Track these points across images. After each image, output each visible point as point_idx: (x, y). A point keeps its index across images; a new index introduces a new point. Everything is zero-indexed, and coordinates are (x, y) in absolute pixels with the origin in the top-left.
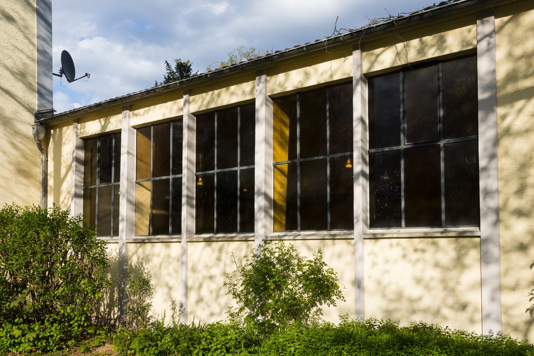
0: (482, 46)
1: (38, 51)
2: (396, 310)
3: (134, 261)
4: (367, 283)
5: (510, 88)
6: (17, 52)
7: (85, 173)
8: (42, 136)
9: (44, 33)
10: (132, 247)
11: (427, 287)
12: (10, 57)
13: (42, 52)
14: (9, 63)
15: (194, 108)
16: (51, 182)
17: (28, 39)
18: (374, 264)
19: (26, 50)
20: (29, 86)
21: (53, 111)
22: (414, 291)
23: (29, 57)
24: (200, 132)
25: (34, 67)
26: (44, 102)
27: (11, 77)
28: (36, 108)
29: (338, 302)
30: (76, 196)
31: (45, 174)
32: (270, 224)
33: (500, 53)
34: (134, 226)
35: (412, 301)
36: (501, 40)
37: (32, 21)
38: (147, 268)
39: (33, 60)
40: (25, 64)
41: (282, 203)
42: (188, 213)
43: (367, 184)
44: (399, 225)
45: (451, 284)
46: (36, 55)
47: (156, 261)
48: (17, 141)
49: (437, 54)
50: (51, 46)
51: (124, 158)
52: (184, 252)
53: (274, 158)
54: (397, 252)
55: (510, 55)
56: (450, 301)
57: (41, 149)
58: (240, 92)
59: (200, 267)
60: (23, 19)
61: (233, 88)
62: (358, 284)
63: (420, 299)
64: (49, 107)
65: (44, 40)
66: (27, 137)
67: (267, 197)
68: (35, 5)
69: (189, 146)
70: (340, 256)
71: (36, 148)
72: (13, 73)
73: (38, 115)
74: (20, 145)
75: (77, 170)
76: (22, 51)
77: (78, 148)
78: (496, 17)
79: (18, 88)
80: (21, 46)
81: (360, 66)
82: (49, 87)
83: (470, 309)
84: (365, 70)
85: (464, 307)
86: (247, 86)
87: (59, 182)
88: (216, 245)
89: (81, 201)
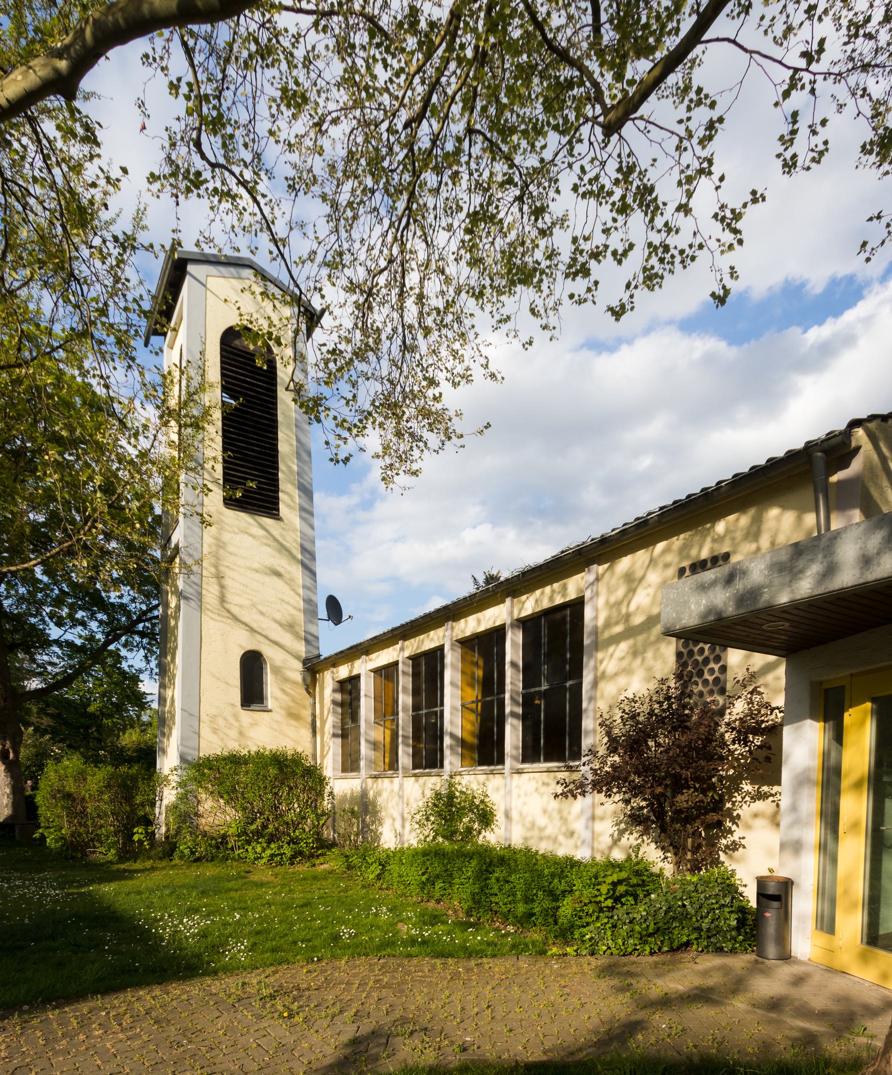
0: (588, 594)
1: (304, 600)
2: (531, 838)
3: (371, 794)
4: (515, 815)
5: (606, 635)
6: (284, 605)
7: (342, 714)
8: (309, 680)
9: (309, 582)
10: (370, 781)
11: (550, 818)
12: (279, 611)
13: (308, 601)
14: (278, 616)
15: (407, 654)
16: (318, 724)
17: (294, 590)
18: (519, 796)
19: (292, 601)
20: (296, 635)
21: (319, 656)
22: (542, 821)
23: (295, 608)
24: (416, 675)
25: (300, 617)
26: (310, 648)
27: (279, 629)
28: (304, 655)
29: (496, 829)
30: (334, 735)
31: (314, 716)
32: (457, 761)
33: (601, 601)
34: (371, 763)
35: (541, 829)
36: (602, 587)
37: (297, 572)
38: (380, 801)
39: (299, 610)
40: (291, 615)
41: (472, 740)
42: (403, 751)
43: (519, 725)
44: (539, 761)
45: (565, 814)
46: (301, 604)
47: (385, 795)
48: (287, 687)
49: (562, 601)
50: (315, 594)
51: (363, 700)
52: (401, 786)
53: (462, 698)
54: (532, 785)
55: (607, 602)
56: (564, 829)
57: (309, 693)
58: (436, 638)
59: (412, 801)
60: (289, 572)
61: (432, 633)
62: (507, 815)
63: (545, 827)
64: (316, 653)
65: (308, 589)
66: (295, 683)
67: (452, 736)
68: (299, 556)
69: (405, 690)
70: (498, 789)
71: (304, 692)
72: (281, 625)
73: (305, 662)
74: (290, 691)
75: (334, 712)
76: (288, 603)
77: (334, 691)
78: (599, 564)
79: (286, 639)
80: (287, 599)
81: (512, 612)
82: (315, 633)
83: (576, 836)
84: (515, 616)
85: (572, 834)
86: (440, 631)
87: (323, 722)
88: (422, 780)
89: (339, 741)
